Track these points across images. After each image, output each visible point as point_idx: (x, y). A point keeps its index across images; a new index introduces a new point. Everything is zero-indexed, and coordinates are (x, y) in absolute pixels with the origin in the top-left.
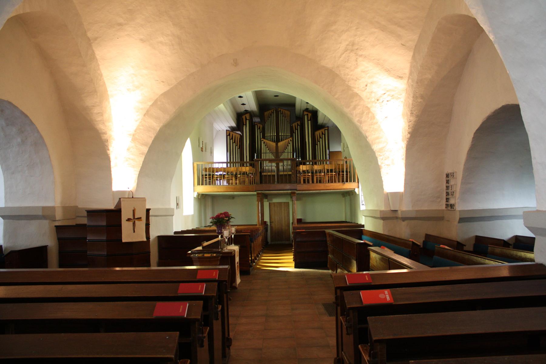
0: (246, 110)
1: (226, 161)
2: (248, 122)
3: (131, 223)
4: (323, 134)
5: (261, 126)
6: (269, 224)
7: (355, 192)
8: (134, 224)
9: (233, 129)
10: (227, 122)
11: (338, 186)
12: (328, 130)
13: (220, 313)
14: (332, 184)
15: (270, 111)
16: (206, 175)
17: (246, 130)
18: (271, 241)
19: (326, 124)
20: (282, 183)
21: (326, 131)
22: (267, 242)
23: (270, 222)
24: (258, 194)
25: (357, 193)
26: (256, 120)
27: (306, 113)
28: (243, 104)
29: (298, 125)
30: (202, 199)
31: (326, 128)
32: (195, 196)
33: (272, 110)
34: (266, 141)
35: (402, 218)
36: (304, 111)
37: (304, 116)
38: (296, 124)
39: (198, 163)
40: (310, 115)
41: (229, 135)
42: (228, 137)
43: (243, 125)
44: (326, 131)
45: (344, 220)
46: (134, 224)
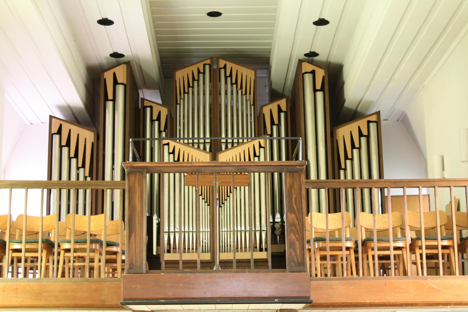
0: (115, 55)
1: (44, 178)
2: (120, 90)
3: (434, 266)
4: (361, 135)
5: (164, 112)
8: (434, 268)
9: (75, 118)
12: (378, 123)
15: (194, 68)
17: (115, 119)
20: (389, 239)
21: (373, 126)
26: (151, 96)
27: (307, 67)
29: (280, 110)
36: (300, 62)
40: (320, 73)
41: (59, 132)
42: (56, 138)
43: (106, 99)
46: (434, 268)
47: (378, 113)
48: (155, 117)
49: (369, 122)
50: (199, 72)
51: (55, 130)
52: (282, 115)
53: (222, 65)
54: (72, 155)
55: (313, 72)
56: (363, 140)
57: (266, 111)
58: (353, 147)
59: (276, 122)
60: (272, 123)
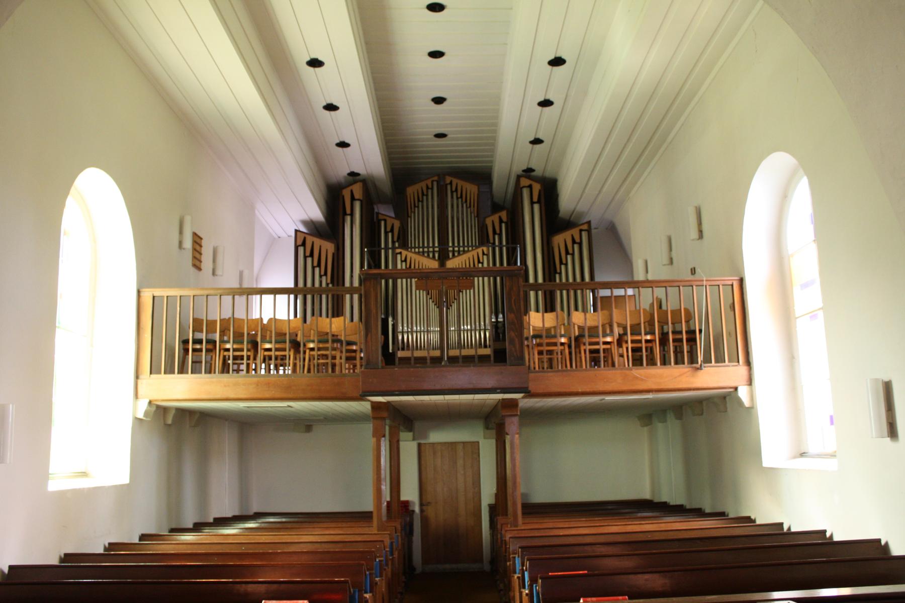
0: (352, 174)
4: (574, 242)
5: (397, 224)
6: (417, 509)
7: (739, 402)
9: (315, 229)
10: (295, 207)
11: (673, 379)
12: (589, 231)
13: (504, 243)
14: (638, 372)
16: (196, 341)
17: (353, 234)
18: (425, 561)
19: (581, 215)
21: (584, 234)
22: (414, 569)
23: (421, 505)
24: (376, 406)
25: (746, 402)
26: (386, 211)
27: (525, 182)
28: (343, 145)
29: (501, 221)
30: (179, 428)
31: (585, 227)
32: (141, 415)
33: (429, 182)
34: (410, 255)
35: (226, 420)
36: (519, 177)
37: (518, 189)
38: (495, 218)
39: (158, 292)
40: (537, 187)
41: (304, 244)
42: (301, 249)
43: (345, 214)
44: (584, 234)
45: (647, 495)
47: (589, 223)
48: (389, 229)
49: (581, 231)
50: (428, 188)
51: (300, 242)
52: (503, 225)
53: (448, 182)
54: (315, 264)
55: (530, 187)
56: (576, 247)
57: (489, 221)
58: (567, 253)
59: (498, 231)
60: (494, 233)
